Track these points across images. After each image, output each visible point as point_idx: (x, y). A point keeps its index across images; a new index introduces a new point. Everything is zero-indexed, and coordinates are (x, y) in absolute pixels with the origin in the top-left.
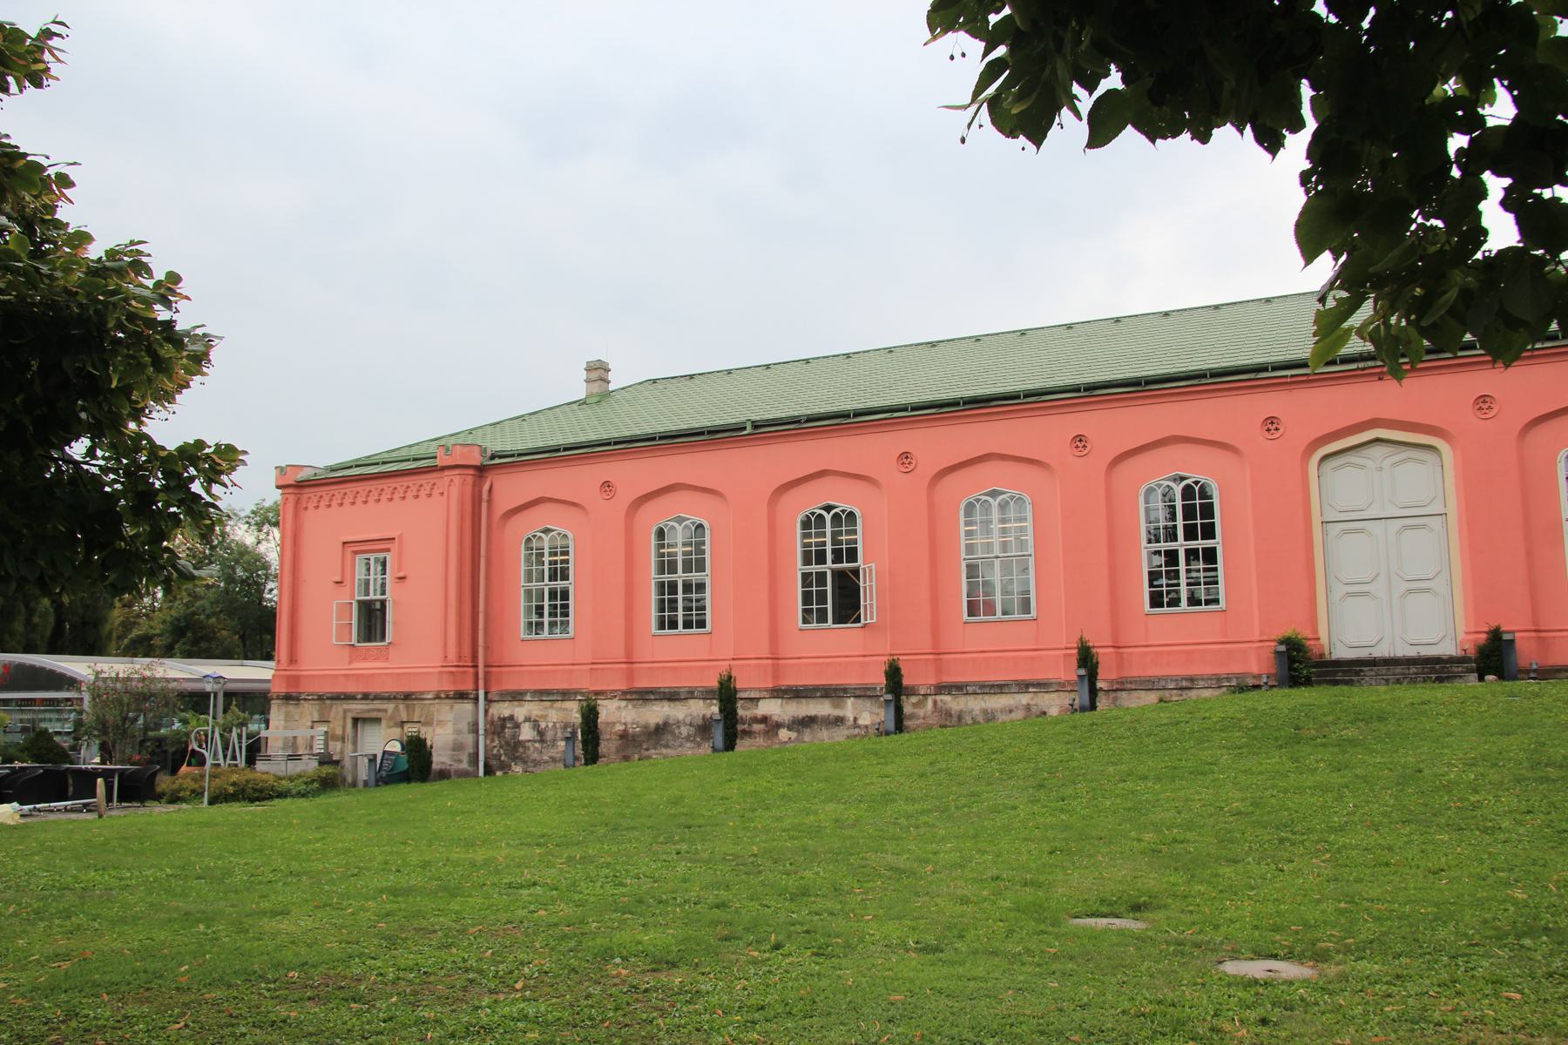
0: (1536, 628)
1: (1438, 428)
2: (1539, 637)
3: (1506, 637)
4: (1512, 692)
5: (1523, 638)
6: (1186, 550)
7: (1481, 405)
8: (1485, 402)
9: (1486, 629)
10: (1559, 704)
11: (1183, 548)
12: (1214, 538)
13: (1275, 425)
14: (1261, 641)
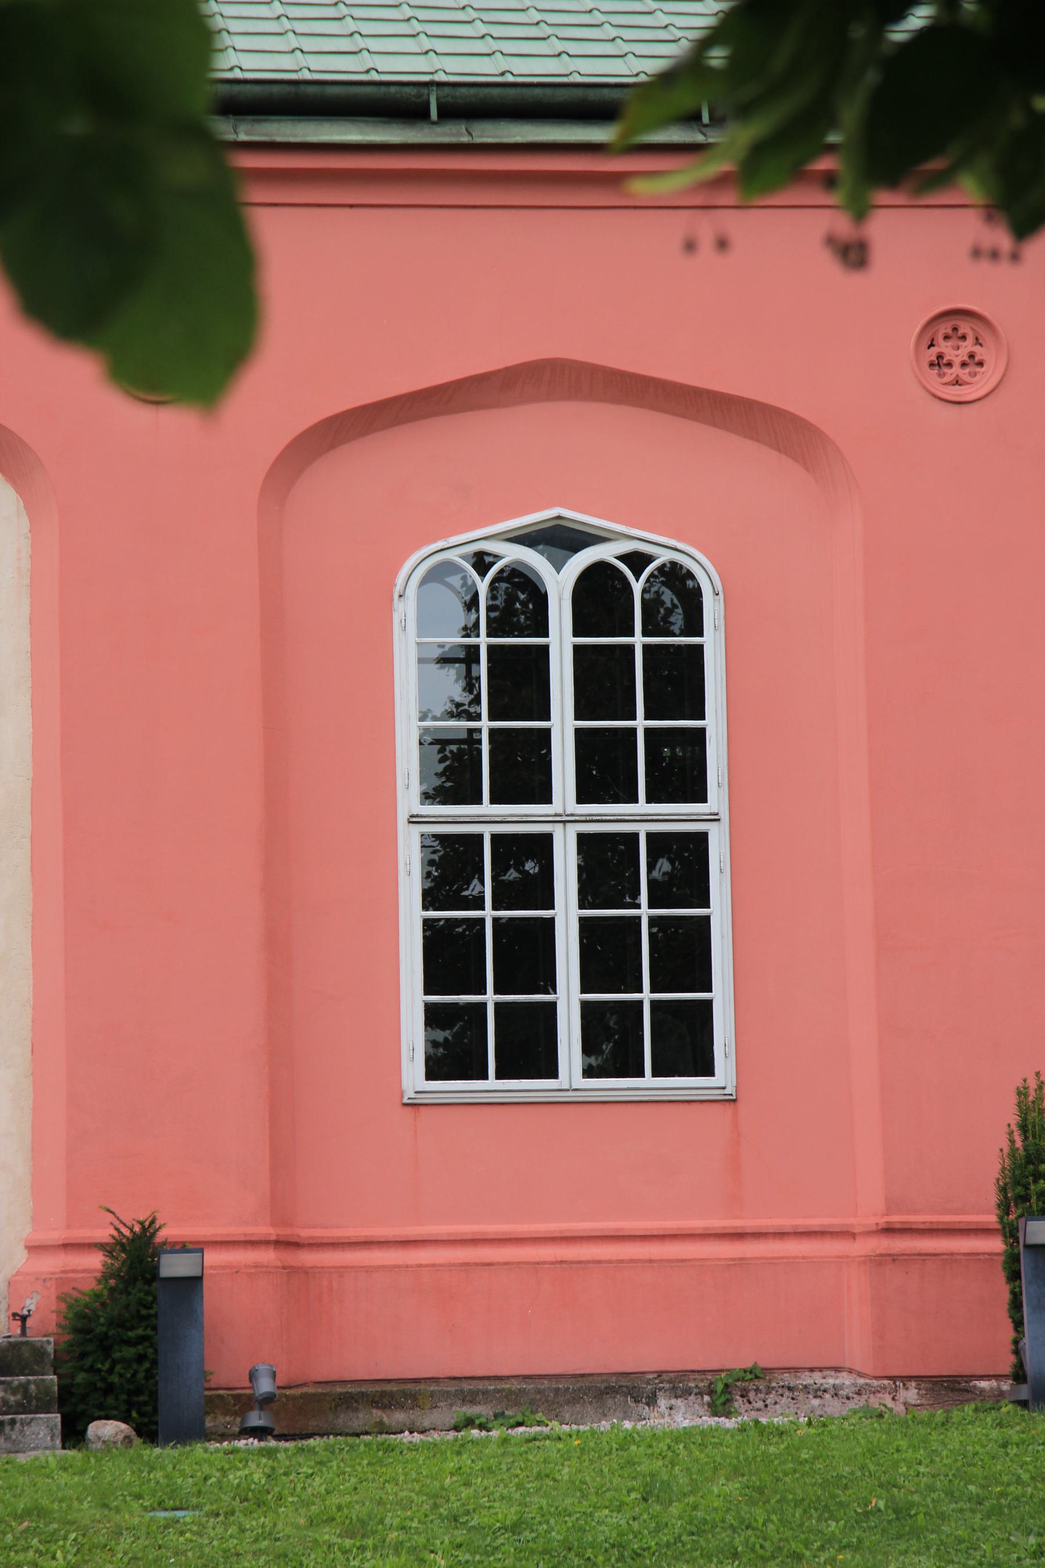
0: (285, 1232)
1: (818, 429)
2: (292, 1271)
3: (173, 1266)
4: (173, 1493)
5: (235, 1271)
6: (583, 840)
7: (944, 347)
8: (956, 335)
9: (104, 1234)
10: (327, 1534)
11: (573, 830)
12: (701, 797)
13: (968, 346)
14: (889, 1230)
